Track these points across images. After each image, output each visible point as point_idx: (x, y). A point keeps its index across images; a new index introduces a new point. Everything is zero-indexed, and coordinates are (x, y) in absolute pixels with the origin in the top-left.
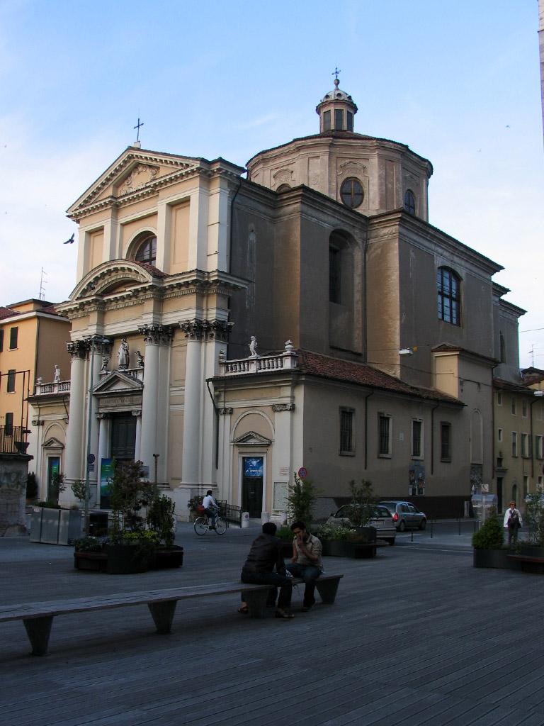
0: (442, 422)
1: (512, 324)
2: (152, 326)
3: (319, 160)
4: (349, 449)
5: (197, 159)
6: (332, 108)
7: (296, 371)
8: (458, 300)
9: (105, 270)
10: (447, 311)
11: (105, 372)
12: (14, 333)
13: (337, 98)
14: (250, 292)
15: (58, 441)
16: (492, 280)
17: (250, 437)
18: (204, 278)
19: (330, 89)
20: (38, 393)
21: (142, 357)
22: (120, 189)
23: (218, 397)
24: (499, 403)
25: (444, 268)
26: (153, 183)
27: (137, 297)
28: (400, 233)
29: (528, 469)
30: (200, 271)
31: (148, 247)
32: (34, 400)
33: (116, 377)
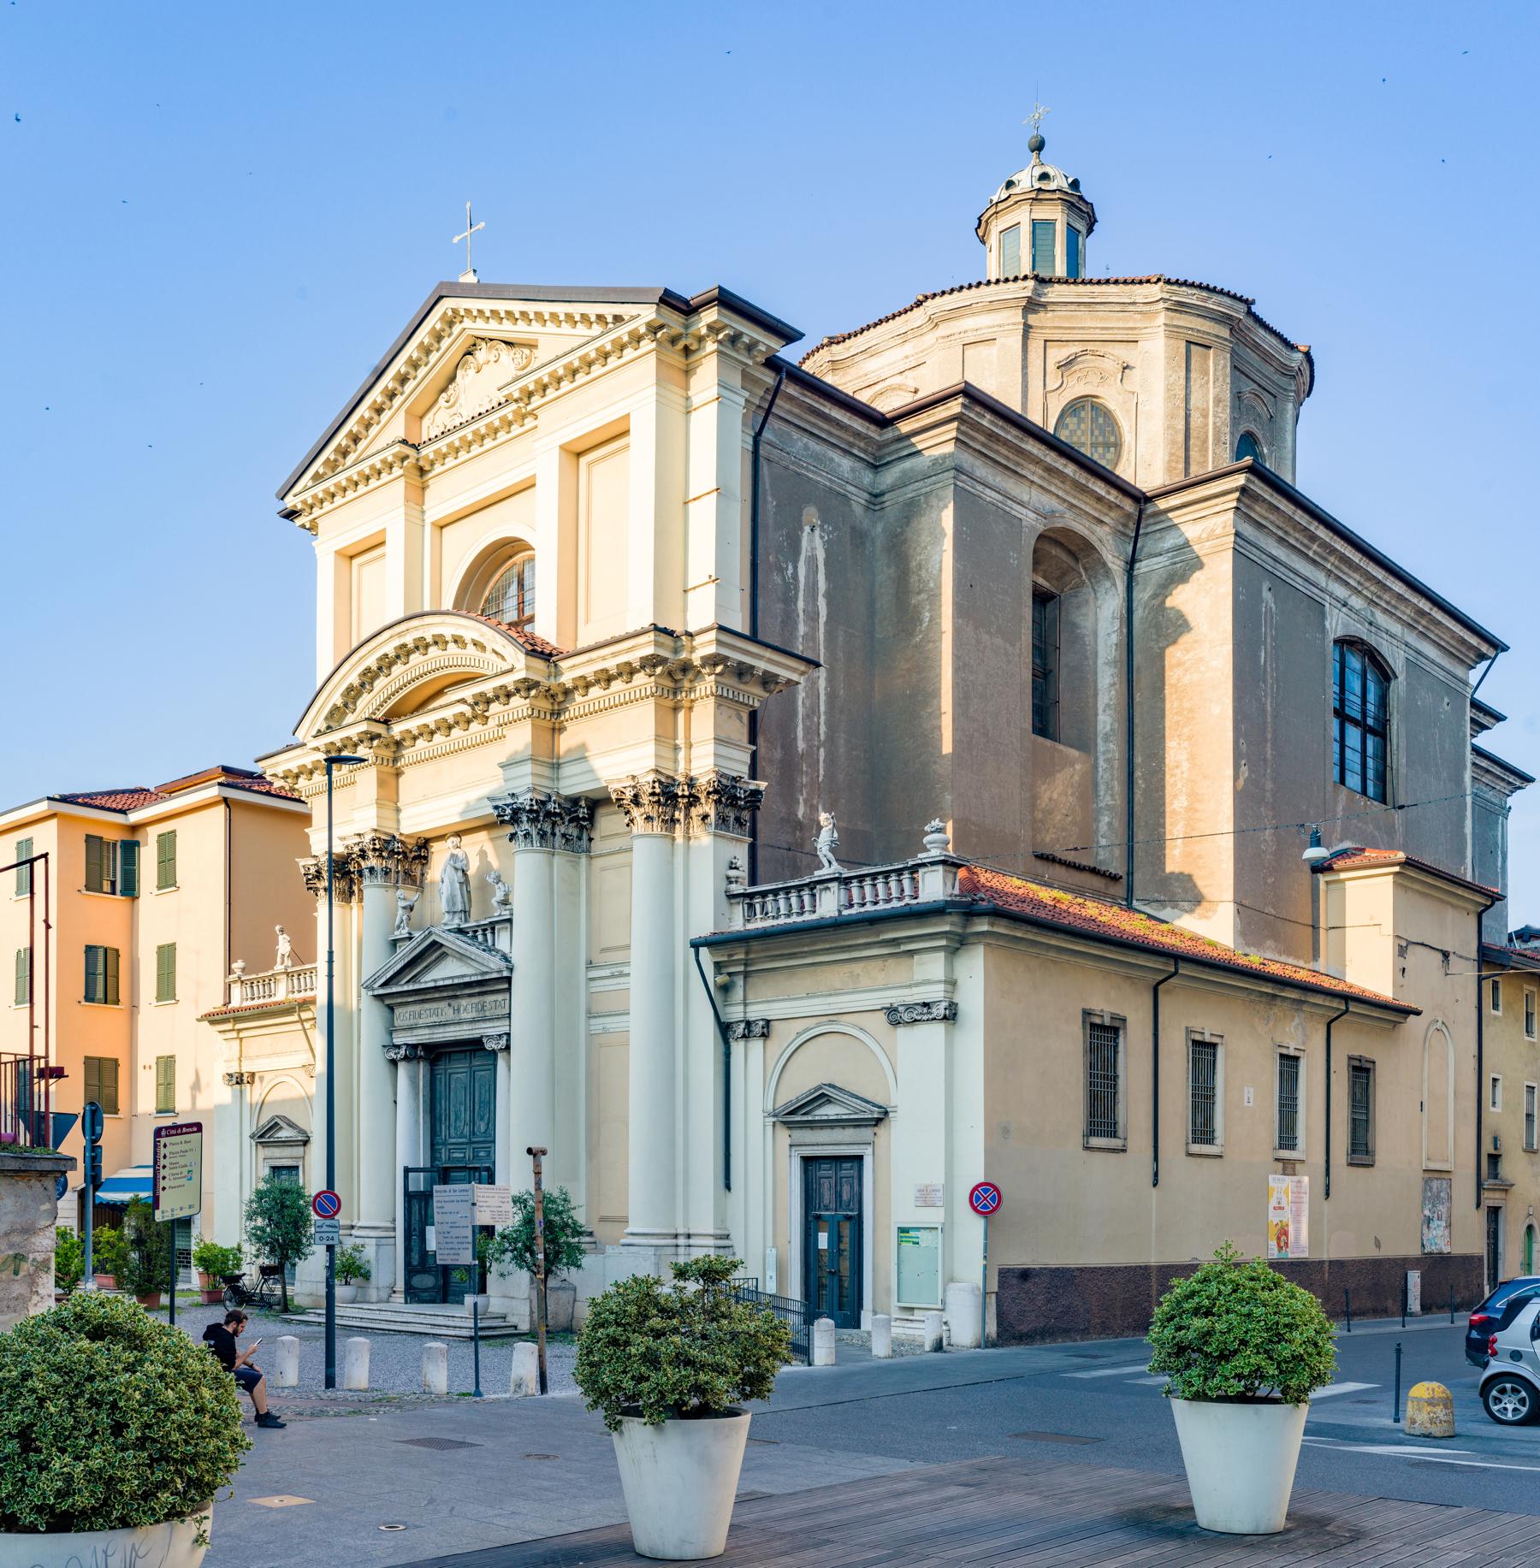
0: (1350, 1058)
2: (529, 796)
8: (1380, 731)
10: (1353, 758)
11: (404, 933)
12: (167, 844)
13: (1037, 185)
15: (292, 1125)
18: (676, 651)
20: (236, 1003)
22: (426, 421)
25: (1347, 643)
28: (1237, 534)
30: (665, 631)
33: (435, 945)
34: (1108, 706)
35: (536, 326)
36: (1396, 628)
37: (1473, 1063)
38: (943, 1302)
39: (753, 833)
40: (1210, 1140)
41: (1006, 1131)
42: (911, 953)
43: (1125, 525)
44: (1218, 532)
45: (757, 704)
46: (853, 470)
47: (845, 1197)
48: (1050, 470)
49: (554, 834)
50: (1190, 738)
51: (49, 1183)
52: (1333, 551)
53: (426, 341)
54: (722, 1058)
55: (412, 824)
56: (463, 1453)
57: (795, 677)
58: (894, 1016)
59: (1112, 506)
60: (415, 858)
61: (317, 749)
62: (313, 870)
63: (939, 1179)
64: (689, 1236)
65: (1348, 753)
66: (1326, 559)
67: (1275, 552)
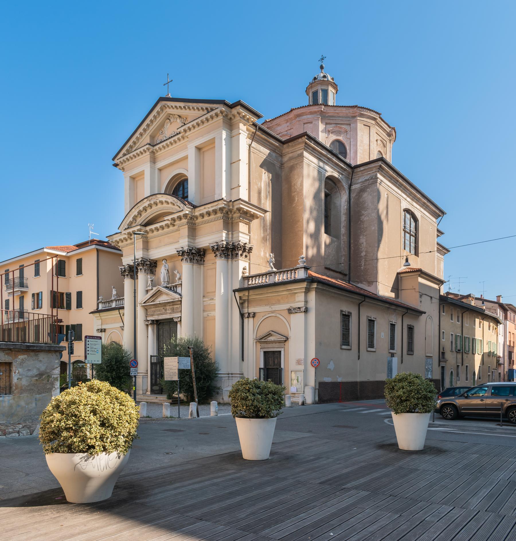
0: (408, 325)
2: (187, 248)
10: (407, 242)
11: (150, 288)
17: (269, 335)
20: (100, 308)
23: (242, 304)
24: (444, 312)
26: (183, 128)
27: (174, 225)
29: (460, 361)
31: (181, 188)
34: (344, 226)
37: (437, 327)
38: (304, 392)
39: (250, 260)
41: (320, 344)
43: (348, 175)
46: (276, 157)
47: (276, 363)
48: (329, 158)
50: (366, 236)
51: (58, 354)
54: (241, 323)
55: (155, 254)
56: (181, 433)
58: (290, 311)
59: (345, 170)
61: (125, 234)
62: (123, 270)
63: (302, 357)
64: (232, 374)
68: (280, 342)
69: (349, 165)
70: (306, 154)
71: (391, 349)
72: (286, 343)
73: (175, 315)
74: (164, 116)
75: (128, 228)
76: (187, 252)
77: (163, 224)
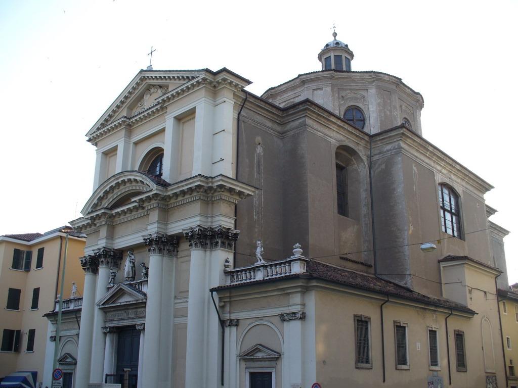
0: (455, 331)
1: (499, 243)
2: (155, 235)
3: (322, 92)
4: (367, 361)
5: (203, 70)
6: (332, 55)
7: (306, 275)
9: (113, 184)
10: (449, 224)
11: (112, 285)
13: (335, 46)
14: (257, 202)
15: (71, 357)
16: (487, 203)
17: (256, 350)
18: (207, 183)
19: (330, 39)
21: (147, 269)
23: (222, 307)
24: (505, 311)
25: (443, 185)
27: (143, 208)
32: (52, 316)
33: (121, 288)
34: (365, 205)
35: (168, 81)
36: (459, 181)
40: (405, 363)
42: (288, 294)
43: (366, 145)
44: (396, 147)
45: (237, 202)
49: (164, 249)
52: (435, 154)
53: (174, 94)
54: (221, 334)
57: (250, 193)
60: (118, 258)
62: (84, 261)
65: (447, 221)
66: (433, 157)
67: (416, 154)
68: (270, 360)
69: (367, 134)
70: (309, 122)
71: (432, 365)
72: (278, 362)
73: (139, 322)
74: (143, 89)
75: (92, 212)
76: (156, 240)
77: (131, 206)
